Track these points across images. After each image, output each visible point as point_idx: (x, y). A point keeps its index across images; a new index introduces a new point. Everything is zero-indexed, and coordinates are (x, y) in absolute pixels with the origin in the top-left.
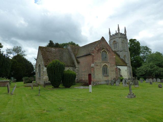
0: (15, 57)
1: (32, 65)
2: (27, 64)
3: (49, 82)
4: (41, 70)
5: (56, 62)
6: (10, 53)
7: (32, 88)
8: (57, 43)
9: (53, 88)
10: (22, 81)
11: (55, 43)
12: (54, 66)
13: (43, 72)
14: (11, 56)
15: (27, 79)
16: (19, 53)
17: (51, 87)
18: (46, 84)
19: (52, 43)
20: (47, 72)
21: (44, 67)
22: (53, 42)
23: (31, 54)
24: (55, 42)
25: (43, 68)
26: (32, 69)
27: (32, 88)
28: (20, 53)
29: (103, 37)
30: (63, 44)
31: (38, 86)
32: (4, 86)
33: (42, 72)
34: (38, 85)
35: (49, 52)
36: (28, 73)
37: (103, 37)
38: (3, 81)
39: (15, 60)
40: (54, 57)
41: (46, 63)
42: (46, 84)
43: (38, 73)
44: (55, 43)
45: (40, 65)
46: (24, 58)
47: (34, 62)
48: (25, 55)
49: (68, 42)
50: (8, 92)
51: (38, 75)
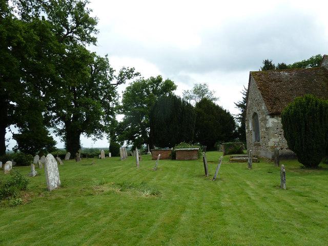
0: (198, 104)
1: (232, 118)
2: (225, 117)
3: (289, 151)
4: (261, 124)
5: (308, 100)
6: (191, 98)
7: (250, 166)
8: (281, 63)
9: (302, 168)
10: (216, 149)
11: (276, 65)
12: (304, 112)
13: (267, 129)
14: (193, 103)
15: (230, 146)
16: (206, 96)
17: (297, 164)
18: (278, 158)
19: (271, 65)
20: (283, 128)
21: (268, 117)
22: (273, 63)
23: (229, 95)
24: (276, 63)
25: (265, 120)
26: (232, 125)
27: (250, 166)
28: (207, 95)
29: (267, 62)
30: (294, 65)
31: (259, 162)
32: (191, 160)
33: (262, 131)
34: (257, 159)
35: (276, 82)
36: (225, 135)
37: (267, 62)
38: (189, 149)
39: (200, 110)
40: (290, 92)
41: (272, 108)
42: (278, 158)
43: (253, 133)
44: (276, 65)
45: (255, 114)
46: (214, 104)
47: (235, 112)
48: (215, 99)
49: (307, 58)
50: (206, 174)
51: (253, 137)
